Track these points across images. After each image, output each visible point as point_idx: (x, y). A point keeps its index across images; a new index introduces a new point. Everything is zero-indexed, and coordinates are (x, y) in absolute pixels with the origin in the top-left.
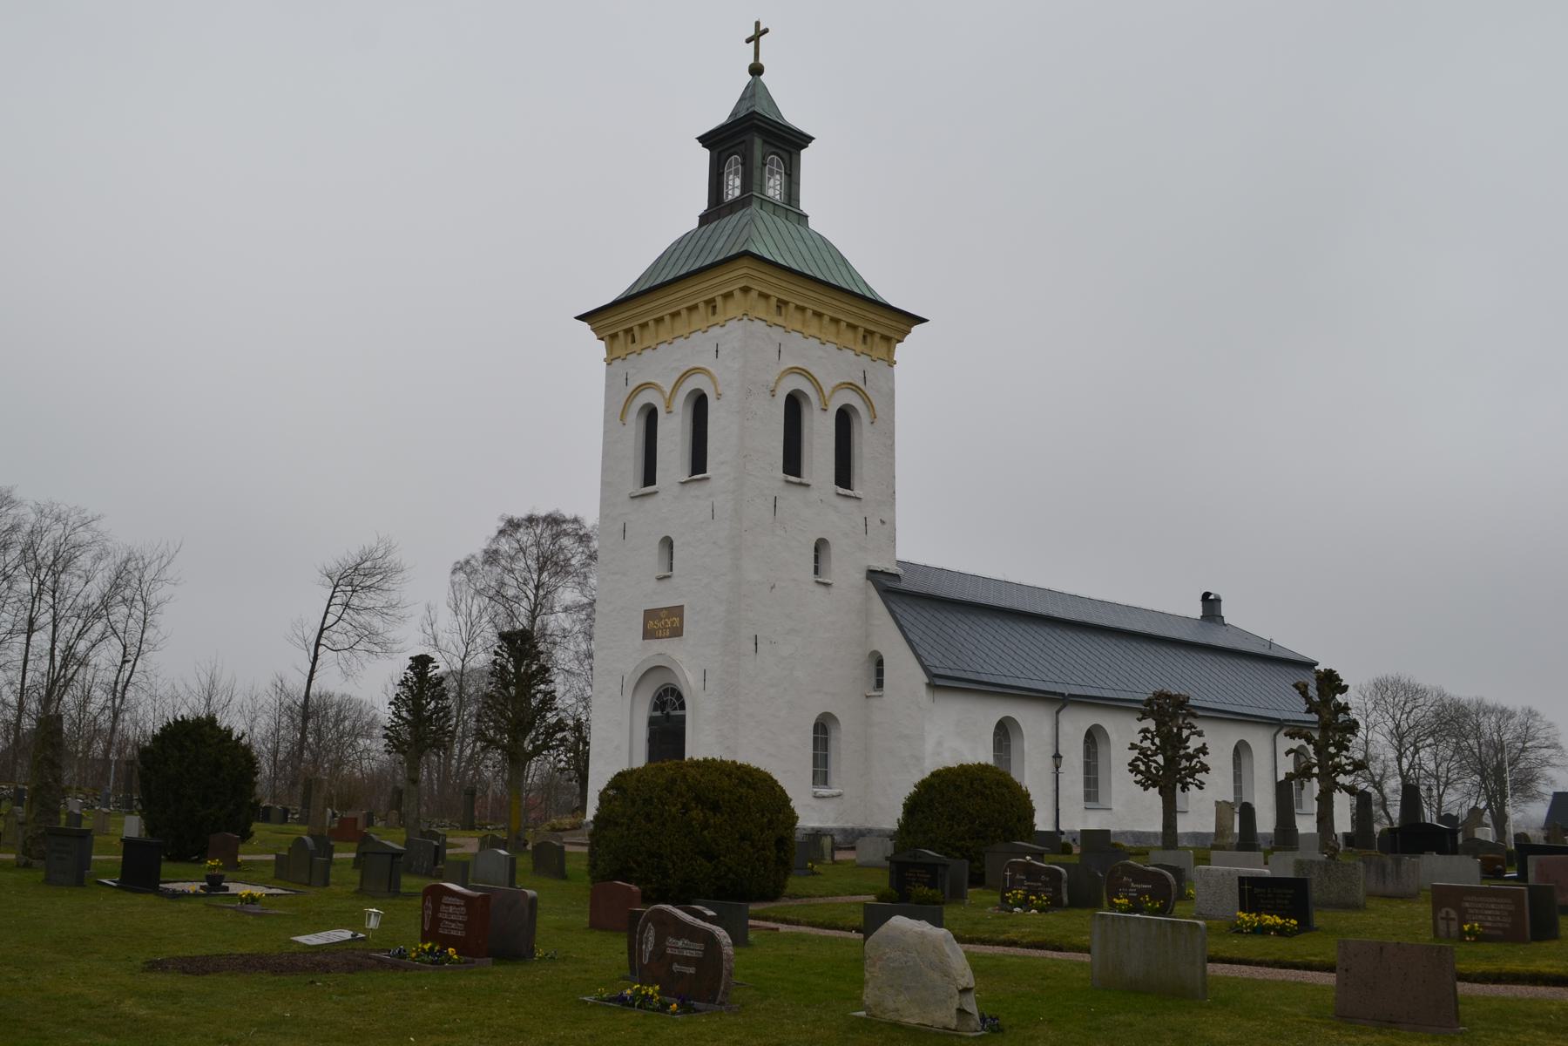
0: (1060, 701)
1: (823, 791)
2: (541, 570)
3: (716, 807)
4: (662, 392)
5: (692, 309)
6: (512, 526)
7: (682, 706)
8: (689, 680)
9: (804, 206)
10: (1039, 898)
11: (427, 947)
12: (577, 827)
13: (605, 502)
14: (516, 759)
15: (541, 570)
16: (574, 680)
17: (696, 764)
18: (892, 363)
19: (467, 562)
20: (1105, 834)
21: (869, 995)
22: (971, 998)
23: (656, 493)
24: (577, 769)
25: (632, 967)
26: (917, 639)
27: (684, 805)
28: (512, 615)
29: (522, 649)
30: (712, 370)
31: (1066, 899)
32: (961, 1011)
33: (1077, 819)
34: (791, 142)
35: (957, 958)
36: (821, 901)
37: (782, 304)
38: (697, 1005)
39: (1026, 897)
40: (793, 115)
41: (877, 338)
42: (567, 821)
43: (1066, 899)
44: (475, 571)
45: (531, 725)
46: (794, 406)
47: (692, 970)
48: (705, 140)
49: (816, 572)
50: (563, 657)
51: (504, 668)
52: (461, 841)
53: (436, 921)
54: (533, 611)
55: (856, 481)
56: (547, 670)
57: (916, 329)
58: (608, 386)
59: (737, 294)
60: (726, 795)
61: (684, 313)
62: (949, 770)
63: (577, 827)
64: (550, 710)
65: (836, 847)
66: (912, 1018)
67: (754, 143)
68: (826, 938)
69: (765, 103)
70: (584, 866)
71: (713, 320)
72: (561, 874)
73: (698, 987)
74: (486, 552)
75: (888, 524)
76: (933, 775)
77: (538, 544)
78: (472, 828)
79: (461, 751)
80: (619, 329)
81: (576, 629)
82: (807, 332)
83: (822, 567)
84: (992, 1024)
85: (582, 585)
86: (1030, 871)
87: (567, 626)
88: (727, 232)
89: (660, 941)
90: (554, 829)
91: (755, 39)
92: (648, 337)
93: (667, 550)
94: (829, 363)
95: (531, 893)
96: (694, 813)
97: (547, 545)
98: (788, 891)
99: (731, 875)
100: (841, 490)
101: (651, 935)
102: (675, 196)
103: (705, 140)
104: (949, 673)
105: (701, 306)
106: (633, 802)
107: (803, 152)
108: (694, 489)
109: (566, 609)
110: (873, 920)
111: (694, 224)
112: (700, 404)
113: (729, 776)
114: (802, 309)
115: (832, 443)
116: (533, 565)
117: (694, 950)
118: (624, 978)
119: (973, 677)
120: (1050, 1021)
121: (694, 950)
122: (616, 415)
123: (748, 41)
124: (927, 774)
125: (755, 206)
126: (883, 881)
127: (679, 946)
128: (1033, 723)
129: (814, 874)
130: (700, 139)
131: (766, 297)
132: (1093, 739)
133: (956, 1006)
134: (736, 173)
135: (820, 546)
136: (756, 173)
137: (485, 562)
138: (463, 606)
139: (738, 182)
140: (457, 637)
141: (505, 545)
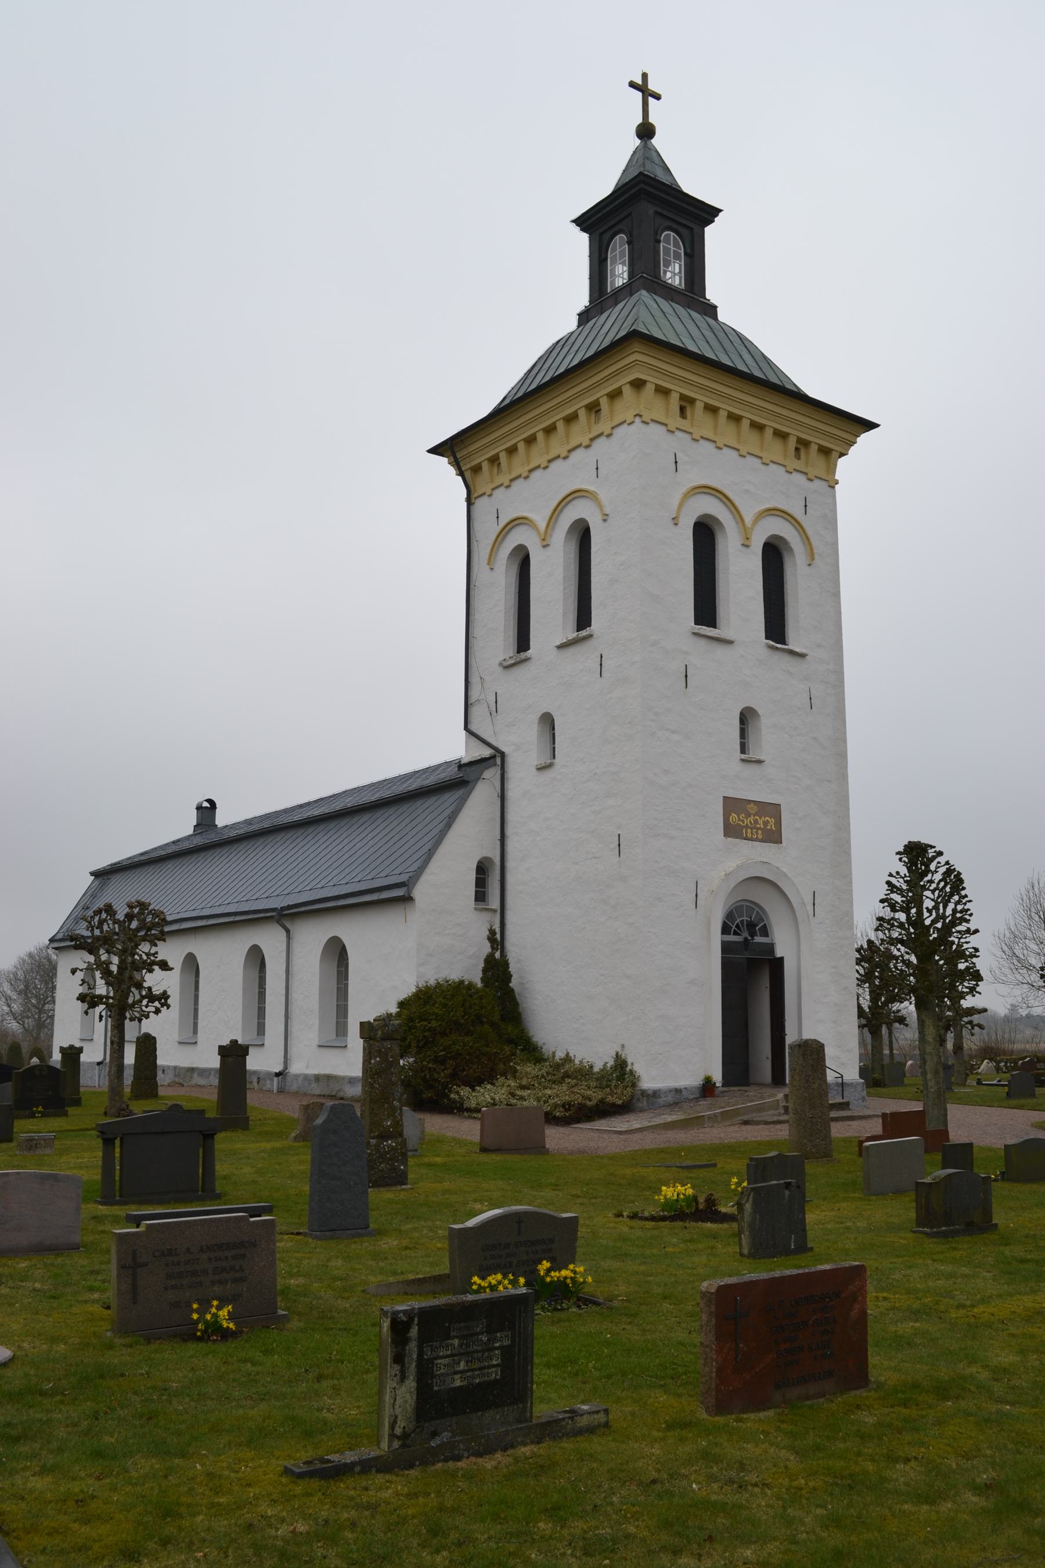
9: (713, 293)
18: (833, 484)
37: (686, 405)
40: (693, 181)
46: (705, 535)
48: (584, 222)
49: (743, 749)
57: (865, 439)
67: (647, 221)
94: (753, 484)
103: (584, 222)
107: (709, 230)
111: (572, 324)
112: (583, 535)
115: (762, 586)
134: (623, 264)
135: (747, 718)
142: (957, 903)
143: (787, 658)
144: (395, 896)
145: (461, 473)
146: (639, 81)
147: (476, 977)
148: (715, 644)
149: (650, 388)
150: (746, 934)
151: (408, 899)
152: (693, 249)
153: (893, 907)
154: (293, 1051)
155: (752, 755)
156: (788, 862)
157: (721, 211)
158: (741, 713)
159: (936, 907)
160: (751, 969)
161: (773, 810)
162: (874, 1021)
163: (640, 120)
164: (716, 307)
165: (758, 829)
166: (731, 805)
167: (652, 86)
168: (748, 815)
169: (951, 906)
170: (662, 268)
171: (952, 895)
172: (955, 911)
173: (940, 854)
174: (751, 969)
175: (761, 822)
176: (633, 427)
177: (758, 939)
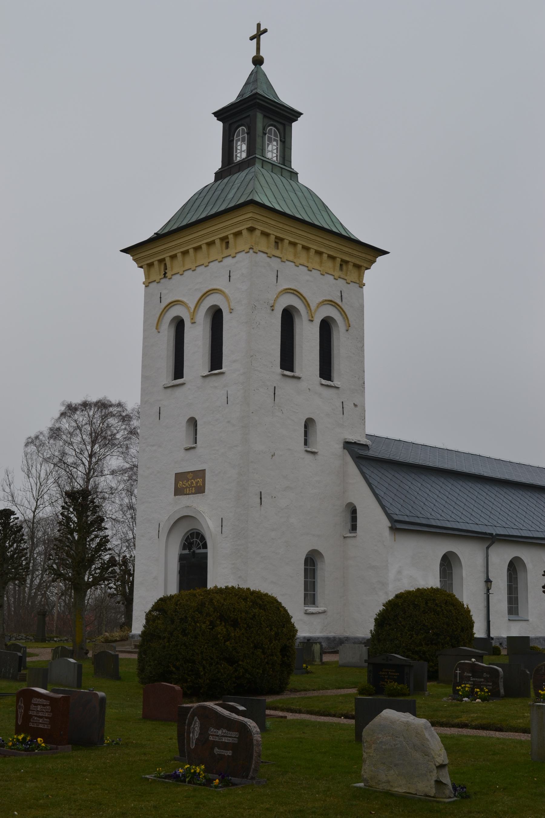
0: (489, 539)
1: (312, 609)
2: (93, 443)
3: (235, 624)
4: (188, 308)
5: (211, 244)
6: (71, 410)
7: (205, 546)
8: (210, 526)
9: (295, 166)
10: (482, 690)
11: (20, 738)
12: (125, 639)
13: (144, 391)
14: (79, 587)
15: (93, 443)
16: (119, 527)
17: (218, 591)
18: (362, 285)
19: (37, 437)
20: (525, 640)
21: (367, 771)
22: (445, 771)
23: (183, 384)
24: (124, 594)
25: (182, 751)
26: (382, 494)
27: (211, 623)
28: (71, 477)
29: (82, 503)
30: (226, 291)
31: (502, 691)
32: (438, 783)
33: (504, 629)
34: (284, 117)
35: (434, 739)
36: (316, 693)
38: (234, 780)
39: (472, 689)
40: (287, 96)
41: (350, 266)
42: (117, 634)
43: (502, 691)
44: (42, 444)
45: (92, 561)
46: (288, 318)
47: (229, 753)
48: (220, 115)
49: (306, 443)
50: (111, 509)
51: (69, 519)
52: (36, 651)
53: (27, 718)
54: (87, 474)
55: (335, 374)
56: (102, 520)
57: (380, 259)
58: (146, 303)
59: (245, 233)
60: (244, 614)
61: (204, 247)
62: (409, 593)
63: (125, 639)
64: (106, 550)
65: (323, 652)
66: (401, 787)
67: (256, 117)
68: (324, 723)
69: (265, 87)
70: (134, 669)
71: (226, 252)
72: (116, 676)
73: (235, 765)
74: (51, 429)
75: (359, 407)
76: (397, 596)
77: (91, 423)
78: (43, 640)
79: (32, 581)
80: (155, 259)
81: (121, 487)
82: (298, 261)
83: (310, 441)
84: (462, 792)
85: (125, 454)
86: (473, 668)
87: (114, 485)
88: (236, 186)
89: (204, 731)
90: (107, 641)
91: (257, 37)
94: (315, 285)
95: (101, 694)
96: (219, 629)
97: (97, 424)
98: (290, 686)
99: (248, 676)
100: (324, 382)
101: (196, 726)
102: (201, 156)
103: (220, 115)
104: (407, 519)
105: (218, 242)
106: (173, 622)
107: (294, 124)
108: (214, 382)
109: (113, 473)
110: (364, 714)
111: (212, 179)
112: (216, 317)
113: (245, 599)
114: (293, 244)
115: (312, 344)
116: (87, 439)
117: (231, 737)
118: (175, 759)
119: (424, 522)
120: (504, 789)
121: (231, 737)
122: (152, 325)
123: (252, 39)
124: (391, 597)
125: (258, 166)
126: (363, 678)
127: (218, 734)
128: (469, 555)
129: (308, 672)
130: (216, 114)
131: (266, 235)
132: (514, 568)
133: (434, 778)
134: (243, 140)
135: (309, 424)
136: (259, 140)
137: (51, 437)
138: (34, 471)
139: (244, 147)
140: (29, 494)
141: (65, 424)
146: (262, 29)
152: (285, 138)
157: (302, 114)
158: (305, 422)
163: (254, 54)
164: (297, 174)
165: (192, 487)
170: (267, 142)
175: (194, 483)
176: (248, 254)
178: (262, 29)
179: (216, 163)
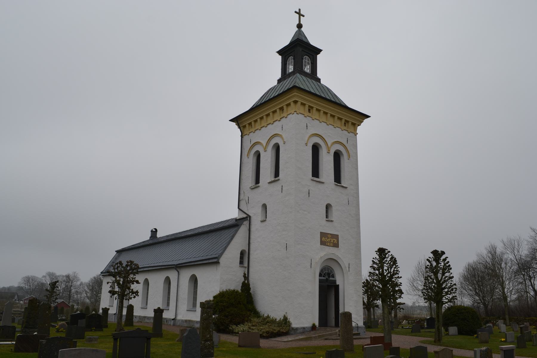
9: (319, 75)
18: (356, 134)
31: (426, 326)
40: (313, 42)
43: (426, 326)
46: (316, 149)
48: (280, 52)
49: (327, 217)
57: (366, 121)
67: (300, 53)
92: (258, 126)
93: (264, 211)
94: (331, 134)
103: (280, 52)
111: (276, 83)
112: (277, 148)
115: (334, 166)
134: (308, 64)
135: (328, 207)
142: (395, 268)
143: (341, 188)
144: (213, 262)
145: (239, 128)
146: (298, 11)
147: (239, 289)
148: (318, 184)
149: (299, 103)
150: (327, 277)
151: (218, 263)
153: (374, 270)
154: (178, 312)
155: (329, 219)
156: (341, 253)
158: (326, 206)
159: (388, 269)
160: (328, 289)
161: (336, 237)
162: (368, 306)
166: (323, 235)
167: (302, 13)
168: (328, 238)
169: (393, 269)
171: (393, 265)
172: (394, 270)
173: (389, 252)
174: (328, 289)
177: (331, 279)
178: (298, 11)
179: (278, 75)
